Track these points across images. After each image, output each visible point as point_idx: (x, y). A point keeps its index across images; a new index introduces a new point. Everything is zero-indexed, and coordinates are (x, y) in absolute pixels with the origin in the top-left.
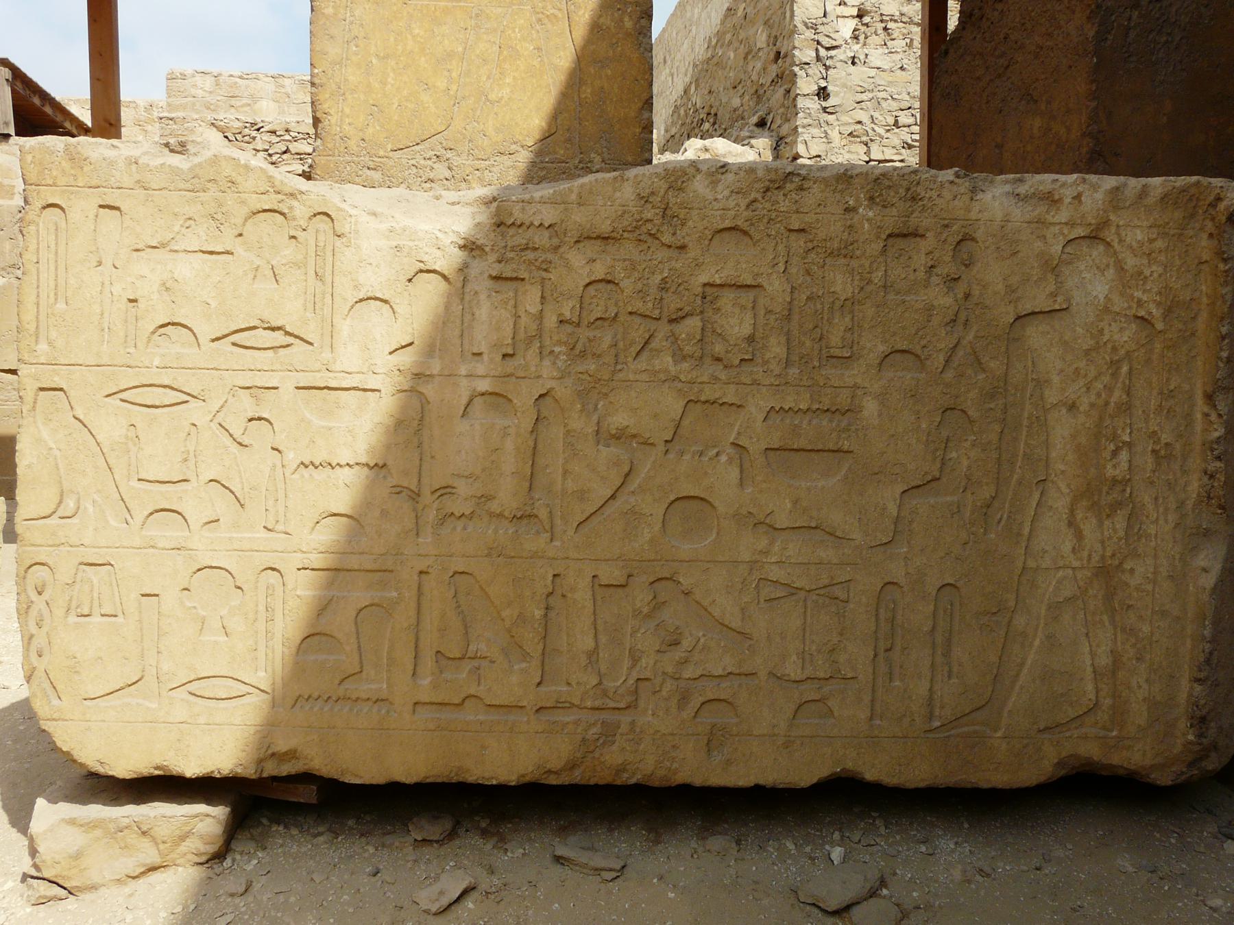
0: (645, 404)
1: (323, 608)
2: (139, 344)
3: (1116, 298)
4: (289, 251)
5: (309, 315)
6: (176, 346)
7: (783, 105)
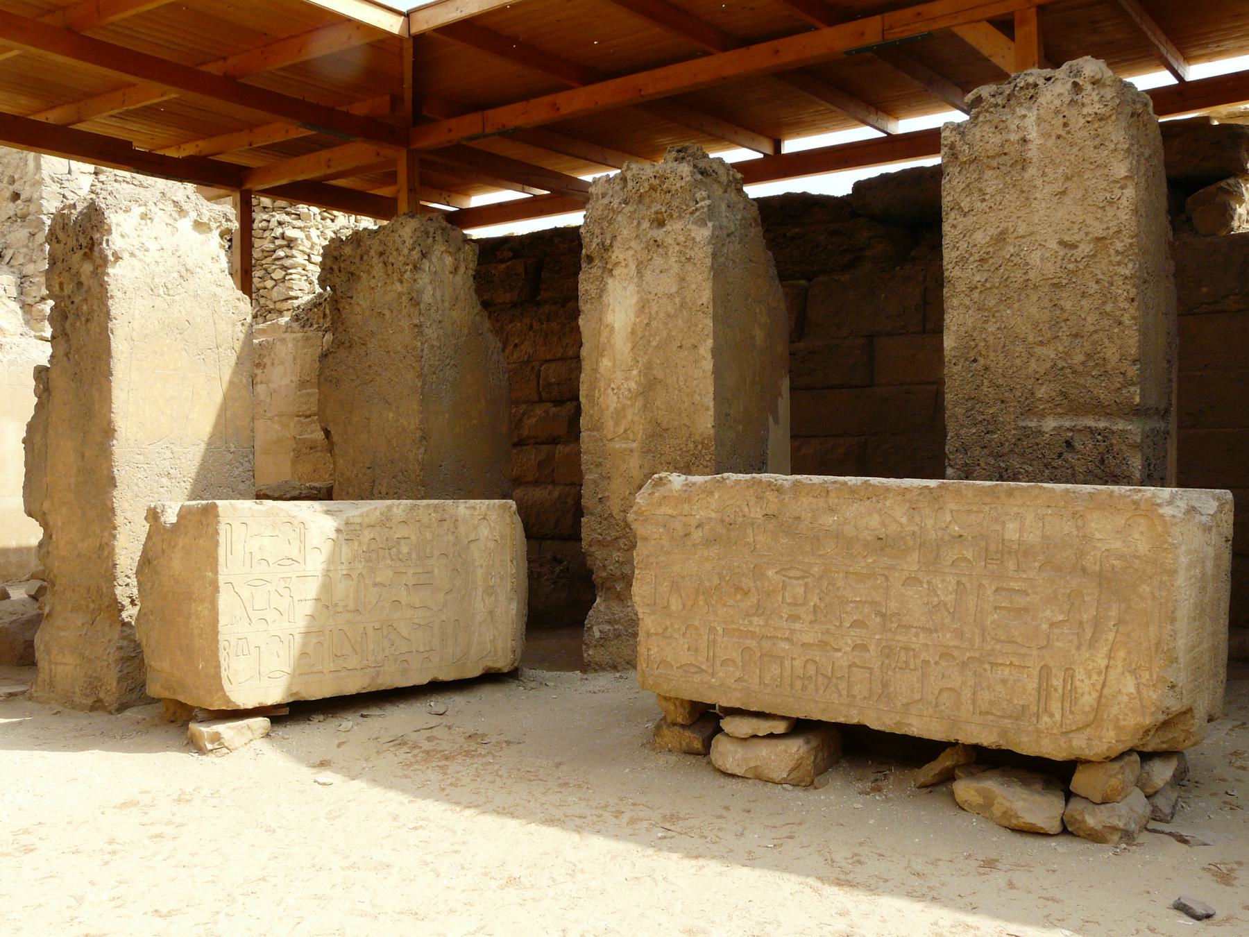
0: (384, 575)
1: (305, 645)
7: (27, 246)
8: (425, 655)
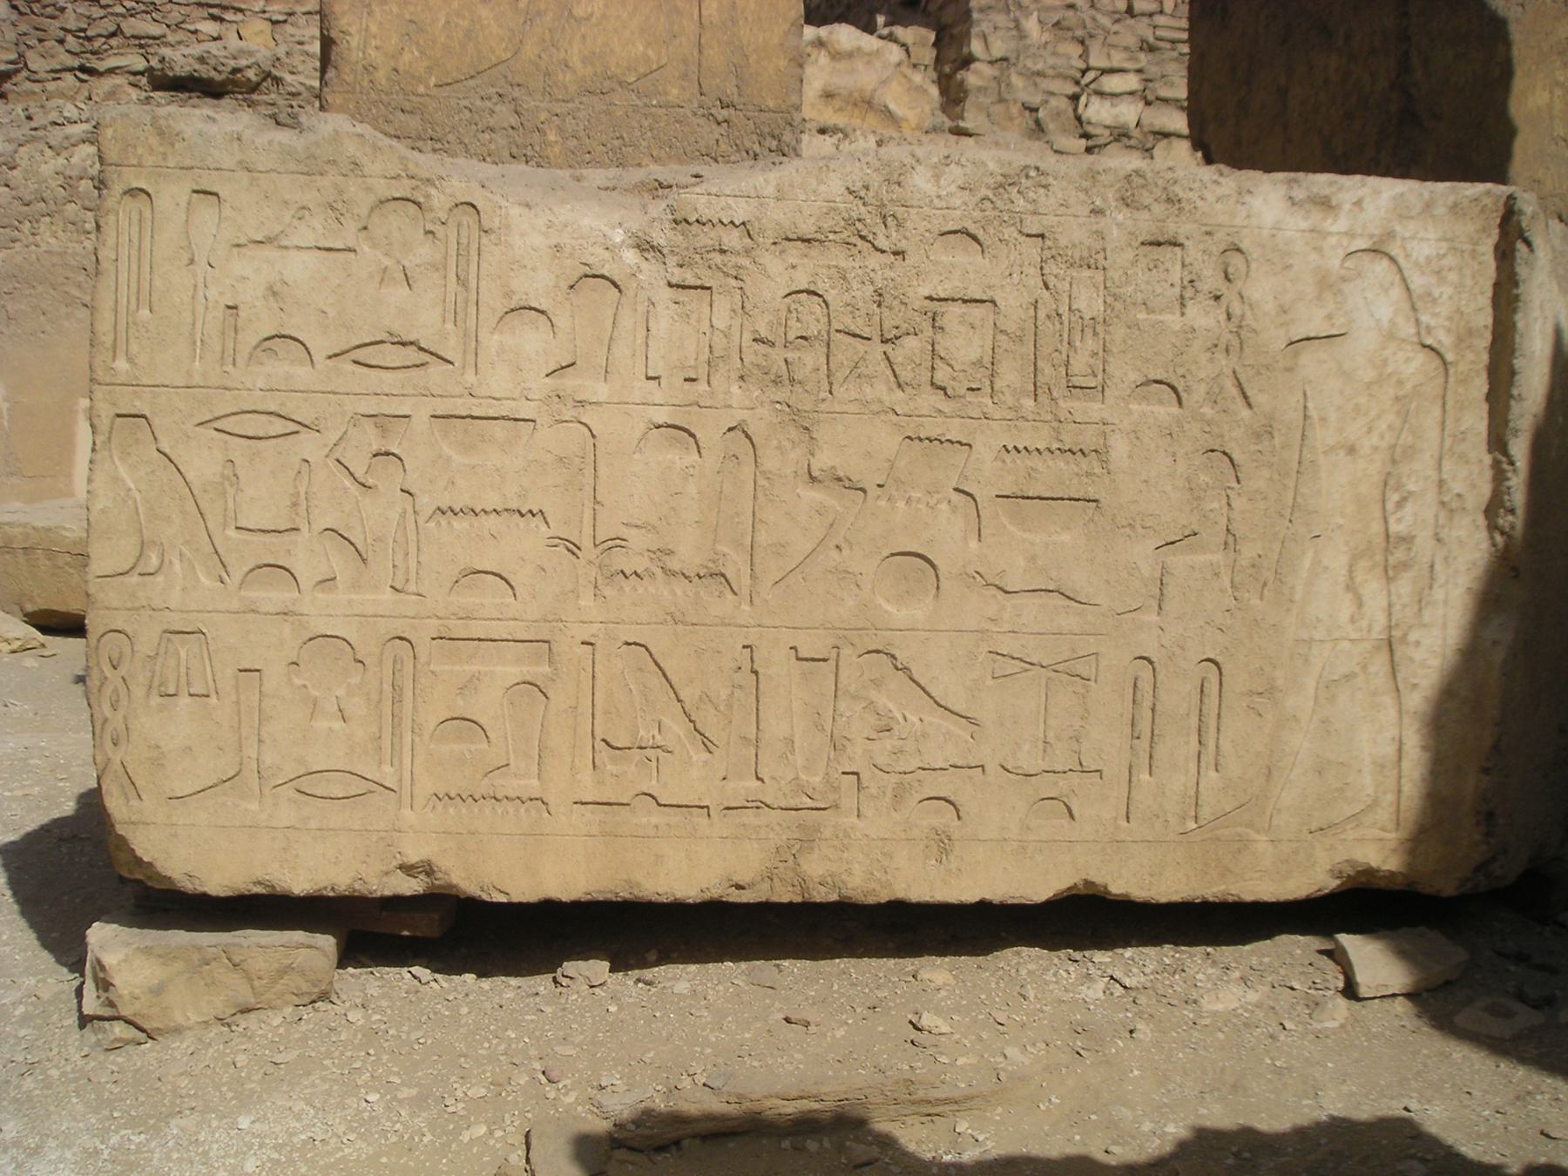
2: (238, 360)
3: (1400, 320)
4: (424, 251)
5: (450, 326)
6: (284, 368)
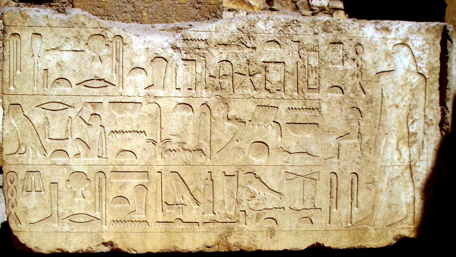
8: (304, 214)
